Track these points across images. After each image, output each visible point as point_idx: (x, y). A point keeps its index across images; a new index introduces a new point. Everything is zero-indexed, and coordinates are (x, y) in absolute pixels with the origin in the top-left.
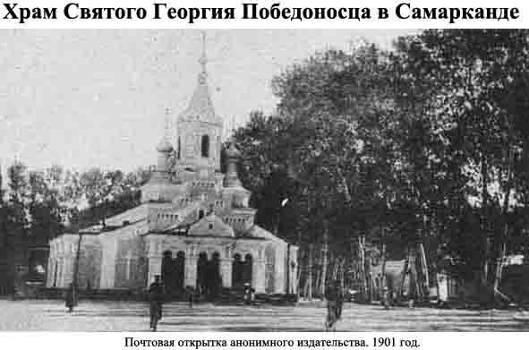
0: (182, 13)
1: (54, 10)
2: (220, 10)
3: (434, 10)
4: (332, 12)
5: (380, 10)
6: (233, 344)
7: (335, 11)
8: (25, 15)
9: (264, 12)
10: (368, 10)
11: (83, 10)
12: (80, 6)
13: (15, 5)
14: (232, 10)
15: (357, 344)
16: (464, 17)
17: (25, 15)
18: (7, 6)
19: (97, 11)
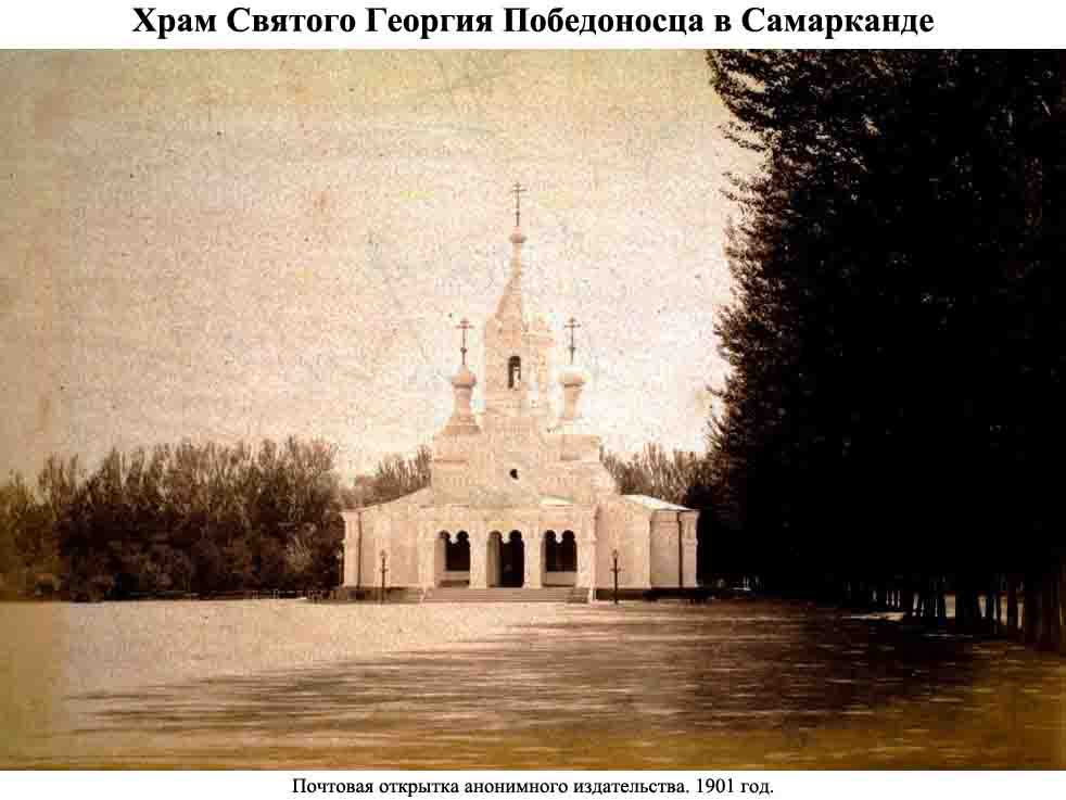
1: (212, 18)
2: (470, 18)
3: (801, 18)
4: (643, 21)
5: (719, 18)
7: (648, 19)
8: (167, 26)
10: (700, 18)
11: (256, 18)
12: (253, 13)
13: (151, 10)
14: (489, 18)
15: (672, 788)
16: (849, 29)
17: (167, 26)
18: (139, 11)
19: (279, 20)
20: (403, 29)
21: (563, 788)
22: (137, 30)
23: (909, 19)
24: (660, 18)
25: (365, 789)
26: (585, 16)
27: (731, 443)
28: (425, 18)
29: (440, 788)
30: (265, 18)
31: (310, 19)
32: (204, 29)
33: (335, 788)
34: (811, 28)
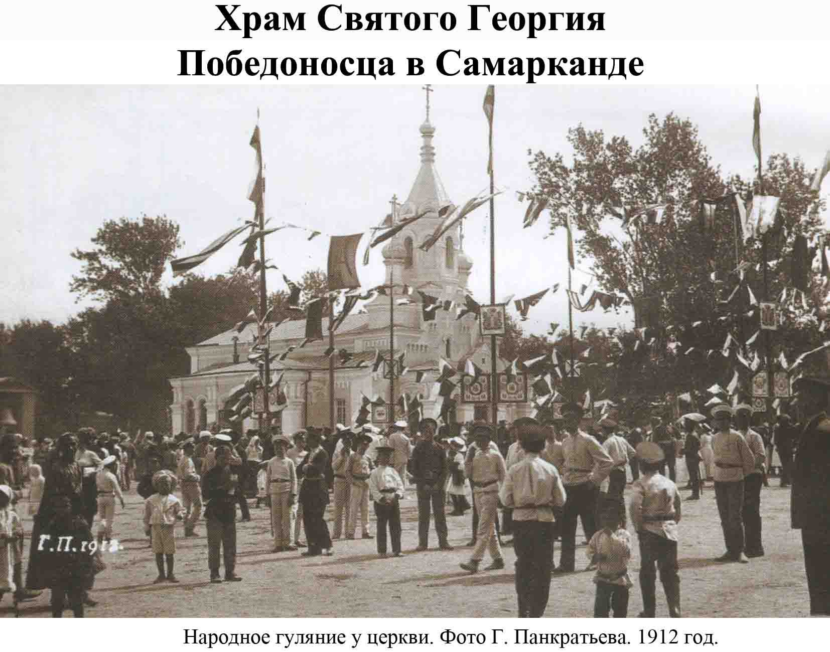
0: (515, 21)
1: (301, 16)
3: (500, 61)
5: (411, 61)
7: (230, 71)
8: (253, 24)
10: (390, 61)
13: (236, 7)
14: (601, 16)
16: (552, 73)
17: (253, 24)
18: (222, 8)
19: (374, 18)
20: (509, 27)
22: (220, 28)
28: (532, 16)
32: (292, 28)
33: (474, 638)
34: (511, 72)
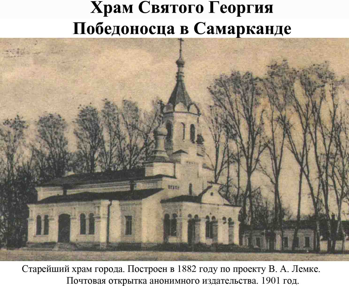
0: (231, 9)
1: (131, 6)
3: (224, 27)
4: (144, 29)
5: (182, 27)
6: (152, 282)
8: (108, 10)
9: (91, 29)
10: (173, 28)
12: (151, 3)
13: (100, 2)
14: (271, 6)
15: (250, 281)
17: (108, 10)
19: (165, 7)
20: (228, 11)
21: (197, 281)
22: (93, 12)
23: (279, 28)
24: (152, 27)
25: (102, 282)
26: (114, 26)
27: (108, 199)
28: (239, 6)
29: (138, 281)
30: (158, 6)
31: (181, 6)
33: (87, 281)
